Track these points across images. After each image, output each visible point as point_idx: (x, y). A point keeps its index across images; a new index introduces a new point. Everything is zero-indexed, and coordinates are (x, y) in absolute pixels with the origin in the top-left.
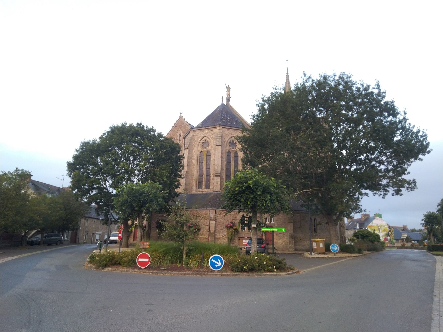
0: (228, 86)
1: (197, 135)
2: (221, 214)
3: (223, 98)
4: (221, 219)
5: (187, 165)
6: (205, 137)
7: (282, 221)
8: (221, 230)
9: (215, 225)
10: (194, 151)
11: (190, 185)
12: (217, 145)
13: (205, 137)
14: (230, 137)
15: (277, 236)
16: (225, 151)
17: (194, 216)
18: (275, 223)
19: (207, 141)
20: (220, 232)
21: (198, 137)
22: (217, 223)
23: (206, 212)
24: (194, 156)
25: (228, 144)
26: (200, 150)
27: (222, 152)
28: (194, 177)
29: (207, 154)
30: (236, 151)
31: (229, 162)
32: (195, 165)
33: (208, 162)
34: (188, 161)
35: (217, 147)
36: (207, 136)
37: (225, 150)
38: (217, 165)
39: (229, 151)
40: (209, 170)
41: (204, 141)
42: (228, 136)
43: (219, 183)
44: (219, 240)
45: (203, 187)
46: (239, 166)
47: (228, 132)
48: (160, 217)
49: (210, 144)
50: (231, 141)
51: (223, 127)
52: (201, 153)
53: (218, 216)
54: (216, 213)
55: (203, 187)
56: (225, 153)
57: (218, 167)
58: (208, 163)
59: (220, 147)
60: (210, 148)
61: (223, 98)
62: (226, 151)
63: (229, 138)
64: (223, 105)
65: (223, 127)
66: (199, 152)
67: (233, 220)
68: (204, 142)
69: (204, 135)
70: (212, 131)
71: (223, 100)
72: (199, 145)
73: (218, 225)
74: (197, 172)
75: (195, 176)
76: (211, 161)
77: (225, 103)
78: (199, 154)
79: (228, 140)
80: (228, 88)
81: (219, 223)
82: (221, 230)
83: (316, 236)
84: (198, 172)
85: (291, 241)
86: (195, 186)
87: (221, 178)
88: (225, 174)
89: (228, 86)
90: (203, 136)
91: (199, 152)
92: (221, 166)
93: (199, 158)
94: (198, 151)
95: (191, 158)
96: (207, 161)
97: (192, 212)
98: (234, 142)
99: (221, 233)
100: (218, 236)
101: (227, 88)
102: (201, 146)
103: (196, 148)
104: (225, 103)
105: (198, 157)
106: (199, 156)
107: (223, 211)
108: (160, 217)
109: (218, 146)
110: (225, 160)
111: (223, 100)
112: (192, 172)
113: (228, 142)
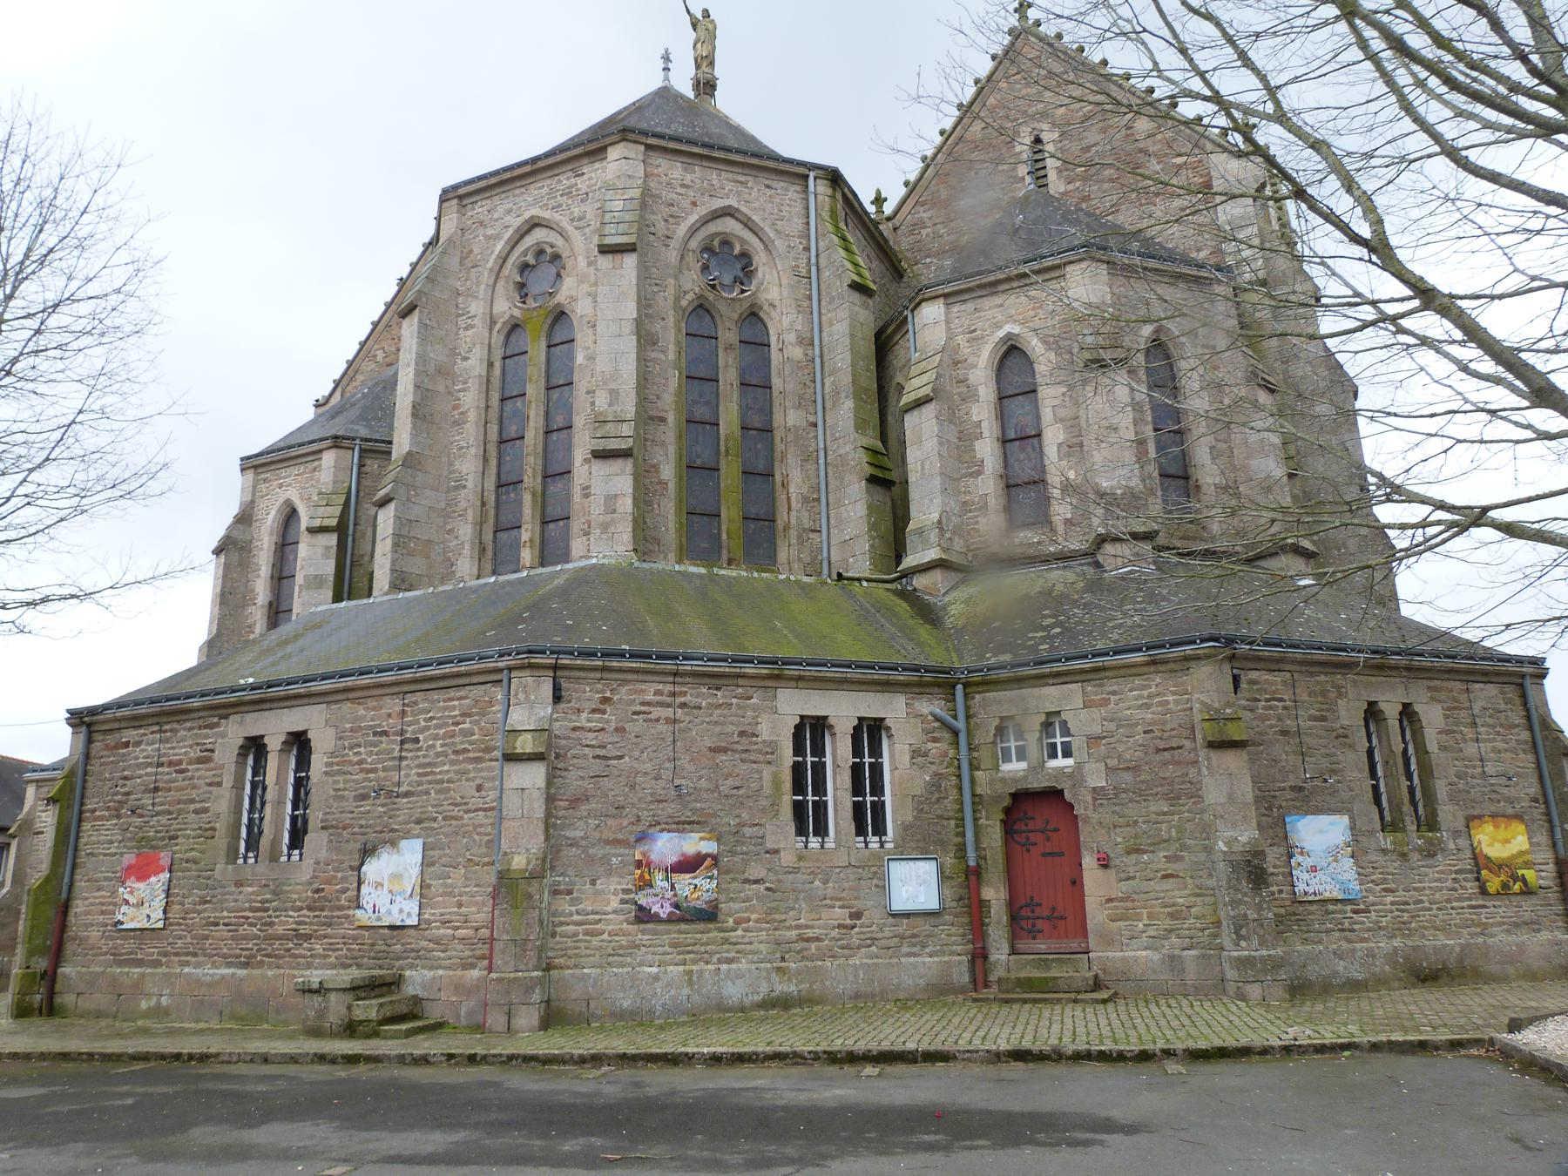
0: (699, 16)
1: (481, 223)
2: (605, 700)
3: (666, 58)
4: (610, 751)
5: (414, 415)
6: (534, 224)
7: (1140, 738)
8: (608, 842)
9: (550, 800)
10: (466, 329)
11: (438, 549)
12: (605, 250)
13: (534, 224)
14: (702, 211)
15: (1112, 872)
16: (671, 302)
17: (385, 733)
18: (1079, 765)
19: (549, 250)
20: (605, 860)
21: (490, 232)
22: (574, 781)
23: (476, 691)
24: (466, 359)
25: (690, 258)
26: (507, 316)
27: (644, 303)
28: (463, 492)
29: (549, 336)
30: (752, 305)
31: (700, 379)
32: (472, 416)
33: (558, 384)
34: (417, 387)
35: (605, 262)
36: (546, 214)
37: (671, 291)
38: (613, 386)
39: (702, 308)
40: (563, 434)
41: (530, 259)
42: (686, 204)
43: (626, 504)
44: (595, 942)
45: (527, 556)
46: (776, 403)
47: (689, 177)
48: (139, 766)
49: (569, 264)
50: (716, 243)
51: (652, 141)
52: (514, 337)
53: (583, 720)
54: (557, 698)
55: (527, 556)
56: (671, 312)
57: (614, 395)
58: (555, 394)
59: (630, 261)
60: (568, 290)
61: (666, 58)
62: (677, 299)
63: (693, 219)
64: (665, 95)
65: (652, 141)
66: (498, 327)
67: (725, 750)
68: (532, 262)
69: (527, 215)
70: (579, 180)
71: (666, 69)
72: (501, 283)
73: (575, 802)
74: (485, 460)
75: (470, 484)
76: (576, 377)
77: (683, 84)
78: (498, 339)
79: (693, 231)
80: (703, 25)
81: (587, 784)
82: (608, 842)
83: (1432, 855)
84: (493, 462)
85: (1252, 915)
86: (467, 551)
87: (635, 466)
88: (672, 449)
89: (699, 16)
90: (519, 221)
91: (498, 327)
92: (644, 380)
93: (498, 365)
94: (493, 322)
95: (444, 372)
96: (554, 382)
97: (371, 703)
98: (737, 251)
99: (609, 873)
100: (587, 906)
101: (694, 26)
102: (512, 286)
103: (476, 308)
104: (683, 84)
105: (490, 365)
106: (498, 354)
107: (625, 682)
108: (139, 766)
109: (619, 256)
110: (672, 356)
111: (666, 69)
112: (451, 464)
113: (694, 244)
